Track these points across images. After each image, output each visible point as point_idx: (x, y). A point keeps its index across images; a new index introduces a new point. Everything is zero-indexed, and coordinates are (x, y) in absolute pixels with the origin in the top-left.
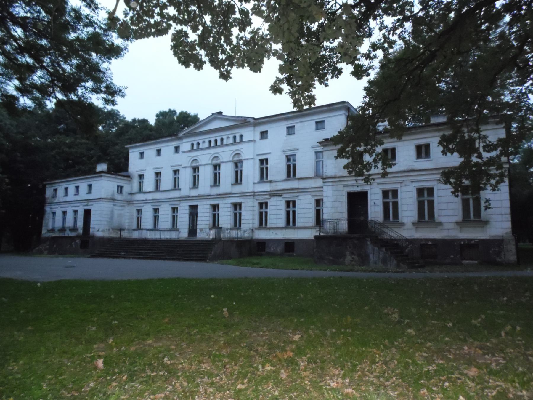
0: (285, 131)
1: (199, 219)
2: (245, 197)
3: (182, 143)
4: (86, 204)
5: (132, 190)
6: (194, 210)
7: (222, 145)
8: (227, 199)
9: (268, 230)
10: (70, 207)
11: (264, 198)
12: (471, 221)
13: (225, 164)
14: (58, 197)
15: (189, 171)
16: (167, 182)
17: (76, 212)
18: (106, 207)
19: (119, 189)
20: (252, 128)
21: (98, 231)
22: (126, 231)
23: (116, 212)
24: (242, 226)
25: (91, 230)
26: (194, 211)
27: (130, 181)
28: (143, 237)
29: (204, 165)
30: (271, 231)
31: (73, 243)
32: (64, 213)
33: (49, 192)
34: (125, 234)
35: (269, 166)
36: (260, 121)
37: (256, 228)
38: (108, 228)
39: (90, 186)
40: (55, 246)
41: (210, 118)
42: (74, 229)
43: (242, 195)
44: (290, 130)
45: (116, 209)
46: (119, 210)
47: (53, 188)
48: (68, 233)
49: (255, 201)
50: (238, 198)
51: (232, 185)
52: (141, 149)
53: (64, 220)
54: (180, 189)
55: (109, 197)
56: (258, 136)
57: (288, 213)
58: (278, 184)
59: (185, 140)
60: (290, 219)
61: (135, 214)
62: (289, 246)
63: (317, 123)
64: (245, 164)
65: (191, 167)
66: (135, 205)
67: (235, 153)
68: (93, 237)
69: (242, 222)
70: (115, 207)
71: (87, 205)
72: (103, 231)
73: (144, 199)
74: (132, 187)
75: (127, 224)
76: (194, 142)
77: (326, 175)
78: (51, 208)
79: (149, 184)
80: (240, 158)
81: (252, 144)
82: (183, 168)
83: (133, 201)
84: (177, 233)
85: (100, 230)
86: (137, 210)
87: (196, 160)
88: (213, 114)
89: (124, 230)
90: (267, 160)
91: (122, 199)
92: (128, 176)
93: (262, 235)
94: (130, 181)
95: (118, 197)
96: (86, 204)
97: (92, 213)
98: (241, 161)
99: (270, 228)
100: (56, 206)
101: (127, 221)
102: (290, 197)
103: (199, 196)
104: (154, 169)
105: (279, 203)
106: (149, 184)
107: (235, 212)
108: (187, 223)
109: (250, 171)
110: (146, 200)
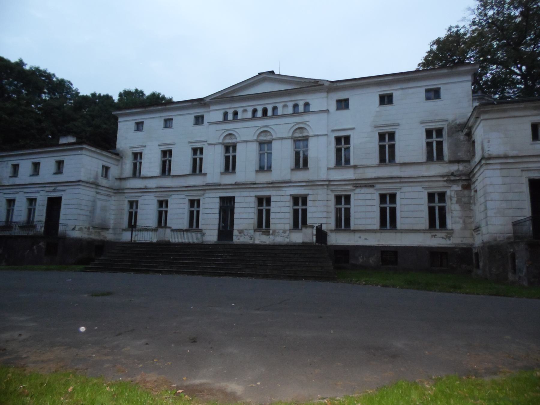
0: (162, 123)
1: (236, 216)
2: (314, 188)
3: (209, 112)
5: (121, 173)
6: (264, 202)
7: (275, 115)
8: (284, 189)
9: (352, 234)
10: (21, 194)
11: (342, 190)
12: (342, 230)
13: (244, 144)
15: (220, 151)
16: (181, 162)
17: (32, 201)
18: (85, 194)
19: (105, 169)
20: (325, 95)
22: (111, 231)
23: (99, 204)
24: (272, 227)
25: (61, 228)
26: (227, 206)
27: (119, 160)
28: (167, 239)
29: (246, 142)
30: (357, 235)
31: (35, 247)
34: (109, 236)
35: (143, 161)
36: (338, 84)
37: (331, 231)
38: (87, 225)
39: (60, 164)
41: (256, 79)
42: (29, 224)
43: (311, 184)
44: (199, 120)
45: (100, 199)
46: (103, 200)
48: (17, 232)
49: (330, 193)
50: (303, 188)
51: (222, 173)
52: (139, 118)
55: (91, 180)
56: (333, 106)
58: (367, 170)
59: (213, 108)
60: (388, 219)
61: (126, 207)
62: (389, 257)
64: (312, 143)
65: (223, 144)
66: (126, 195)
67: (297, 126)
68: (64, 238)
69: (272, 221)
70: (99, 196)
71: (54, 191)
72: (81, 229)
74: (122, 169)
75: (112, 222)
76: (228, 111)
77: (489, 155)
79: (151, 165)
80: (305, 134)
81: (325, 115)
82: (209, 145)
84: (199, 235)
85: (77, 228)
86: (129, 201)
87: (230, 134)
88: (260, 74)
90: (170, 152)
91: (107, 186)
92: (117, 154)
94: (119, 160)
95: (103, 182)
96: (53, 188)
97: (63, 202)
98: (306, 139)
99: (355, 231)
101: (112, 217)
102: (387, 189)
103: (236, 184)
104: (160, 145)
105: (369, 196)
106: (151, 165)
107: (296, 207)
108: (217, 222)
109: (321, 152)
110: (146, 188)
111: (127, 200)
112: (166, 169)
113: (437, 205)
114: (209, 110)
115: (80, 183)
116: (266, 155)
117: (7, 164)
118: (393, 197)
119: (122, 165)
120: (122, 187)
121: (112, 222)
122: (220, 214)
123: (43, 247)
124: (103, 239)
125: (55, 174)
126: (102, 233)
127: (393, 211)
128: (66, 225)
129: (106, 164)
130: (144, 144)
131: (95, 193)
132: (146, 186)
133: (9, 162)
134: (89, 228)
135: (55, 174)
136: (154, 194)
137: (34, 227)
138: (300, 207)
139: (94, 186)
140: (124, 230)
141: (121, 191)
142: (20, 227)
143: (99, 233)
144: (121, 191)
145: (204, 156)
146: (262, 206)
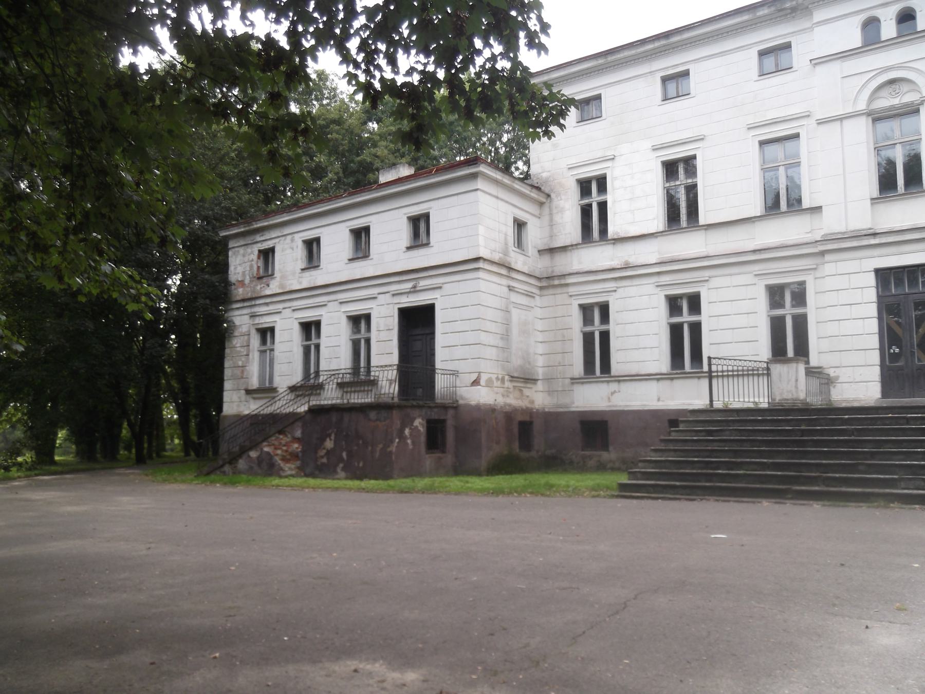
4: (409, 285)
10: (287, 313)
14: (277, 274)
17: (360, 321)
21: (476, 383)
22: (540, 386)
23: (516, 315)
25: (441, 383)
32: (310, 328)
33: (241, 263)
34: (539, 398)
39: (361, 235)
40: (329, 444)
42: (360, 375)
45: (517, 305)
47: (256, 249)
53: (310, 352)
54: (819, 208)
57: (676, 332)
63: (665, 80)
66: (572, 290)
68: (454, 406)
70: (514, 297)
71: (414, 290)
73: (616, 263)
75: (540, 362)
78: (253, 316)
79: (637, 203)
82: (821, 122)
83: (564, 276)
85: (482, 382)
86: (581, 306)
87: (892, 82)
89: (534, 381)
91: (525, 270)
93: (594, 398)
95: (518, 261)
96: (409, 285)
97: (440, 316)
100: (272, 308)
104: (655, 149)
106: (637, 203)
111: (576, 303)
112: (681, 211)
113: (788, 311)
114: (806, 24)
115: (481, 264)
116: (782, 169)
117: (292, 240)
118: (695, 302)
119: (551, 214)
120: (558, 270)
121: (540, 362)
122: (880, 318)
123: (421, 429)
124: (529, 406)
125: (409, 248)
126: (527, 392)
127: (801, 324)
128: (455, 373)
129: (523, 216)
130: (609, 153)
131: (506, 289)
132: (627, 263)
133: (297, 236)
134: (503, 380)
135: (409, 248)
136: (654, 279)
137: (374, 383)
138: (686, 317)
139: (504, 271)
140: (574, 380)
141: (556, 282)
142: (341, 385)
143: (521, 391)
144: (556, 282)
145: (610, 198)
146: (781, 305)
